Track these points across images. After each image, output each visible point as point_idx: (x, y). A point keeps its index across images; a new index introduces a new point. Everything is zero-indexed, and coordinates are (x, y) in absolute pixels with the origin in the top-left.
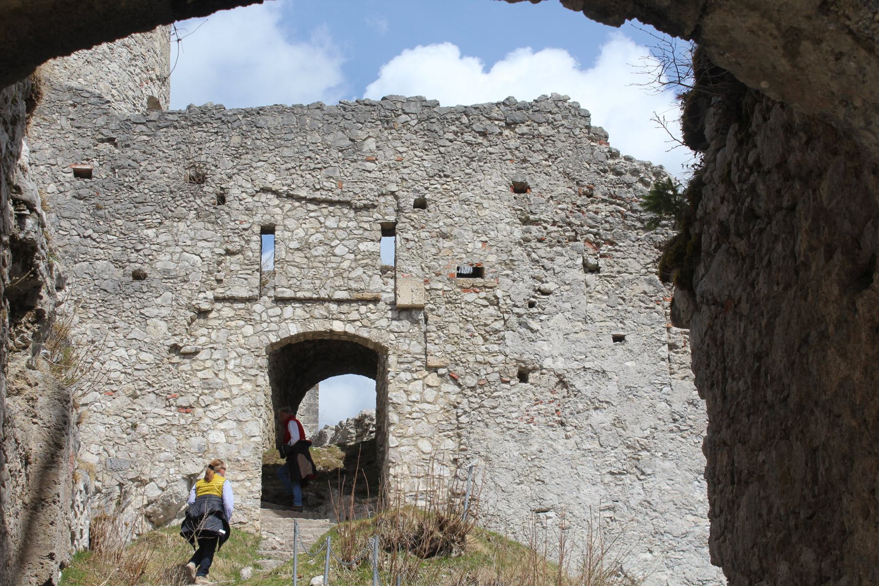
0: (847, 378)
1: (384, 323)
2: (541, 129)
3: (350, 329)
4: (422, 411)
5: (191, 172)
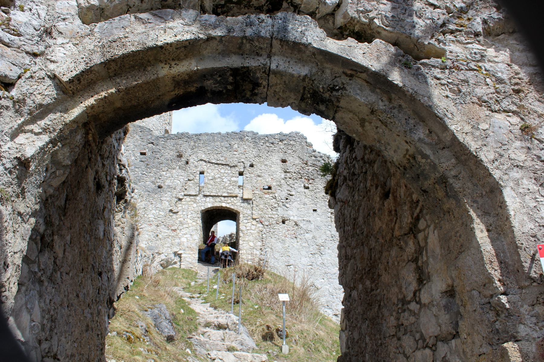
0: (381, 227)
1: (239, 204)
2: (291, 142)
3: (228, 206)
4: (250, 233)
5: (178, 154)
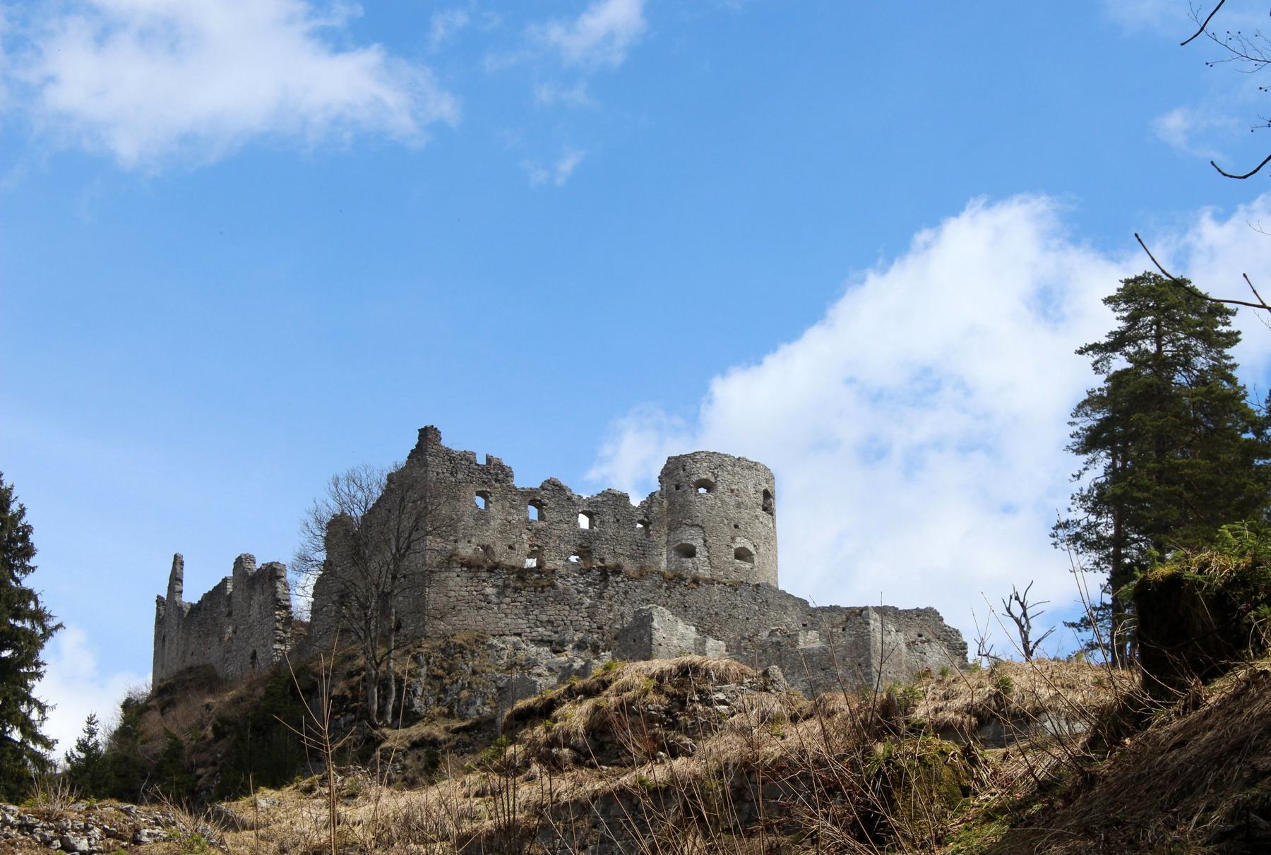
2: (926, 618)
